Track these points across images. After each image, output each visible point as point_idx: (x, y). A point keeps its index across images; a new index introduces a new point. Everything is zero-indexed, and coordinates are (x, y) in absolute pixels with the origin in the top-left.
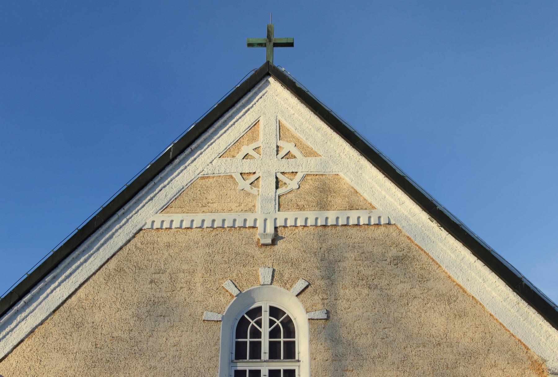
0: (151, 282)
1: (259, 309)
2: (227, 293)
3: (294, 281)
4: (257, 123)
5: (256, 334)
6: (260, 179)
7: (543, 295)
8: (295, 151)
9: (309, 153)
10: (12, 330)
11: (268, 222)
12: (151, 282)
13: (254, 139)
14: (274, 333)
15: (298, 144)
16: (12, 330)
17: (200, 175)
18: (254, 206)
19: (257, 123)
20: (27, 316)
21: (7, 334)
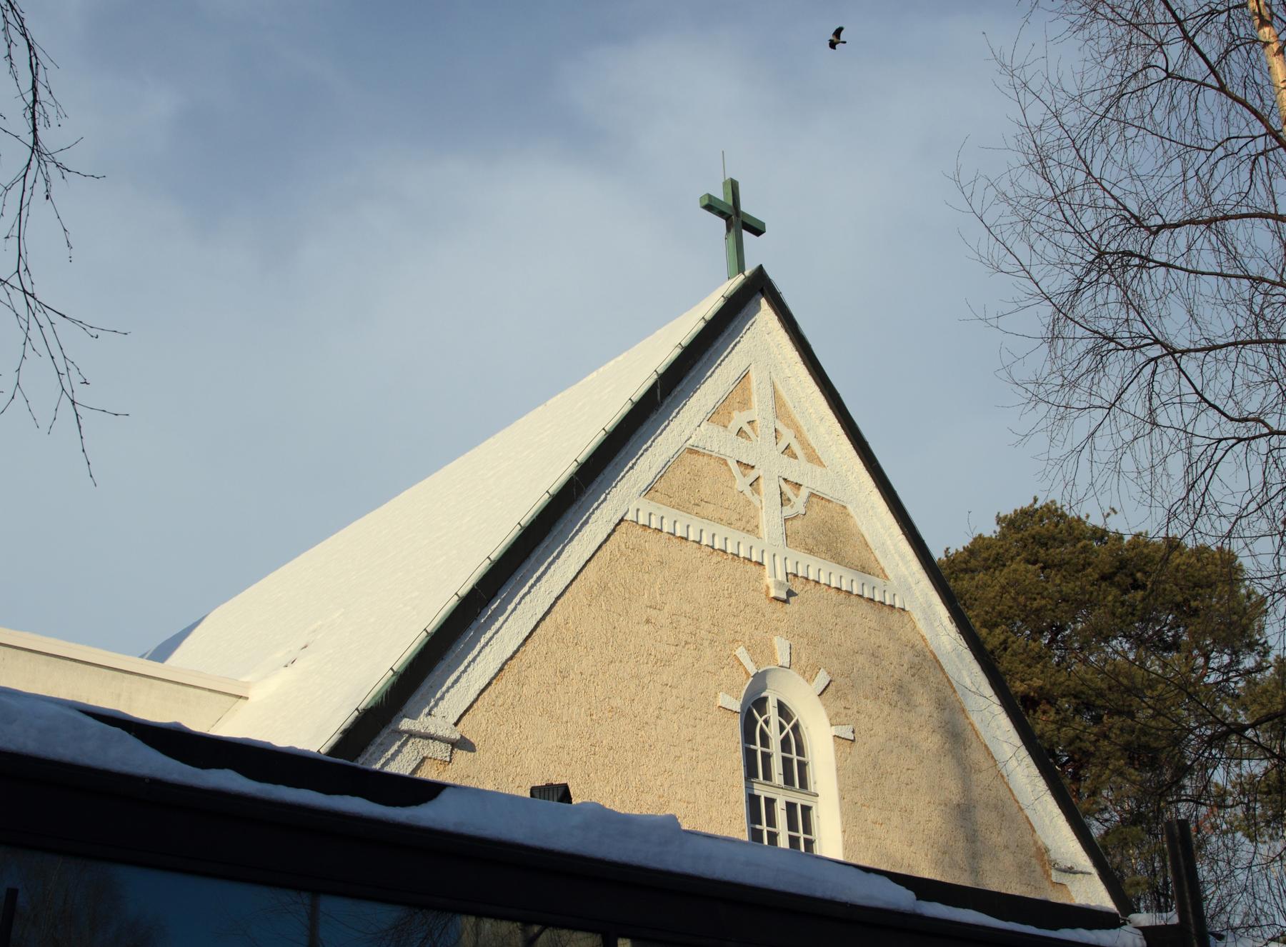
0: (648, 621)
1: (765, 699)
2: (741, 669)
3: (816, 669)
4: (745, 376)
5: (765, 740)
6: (761, 481)
7: (608, 484)
8: (796, 448)
9: (814, 458)
10: (474, 660)
11: (777, 558)
12: (648, 621)
13: (745, 404)
14: (785, 744)
15: (805, 444)
16: (474, 660)
17: (687, 445)
18: (757, 527)
19: (745, 376)
20: (491, 638)
21: (469, 665)
